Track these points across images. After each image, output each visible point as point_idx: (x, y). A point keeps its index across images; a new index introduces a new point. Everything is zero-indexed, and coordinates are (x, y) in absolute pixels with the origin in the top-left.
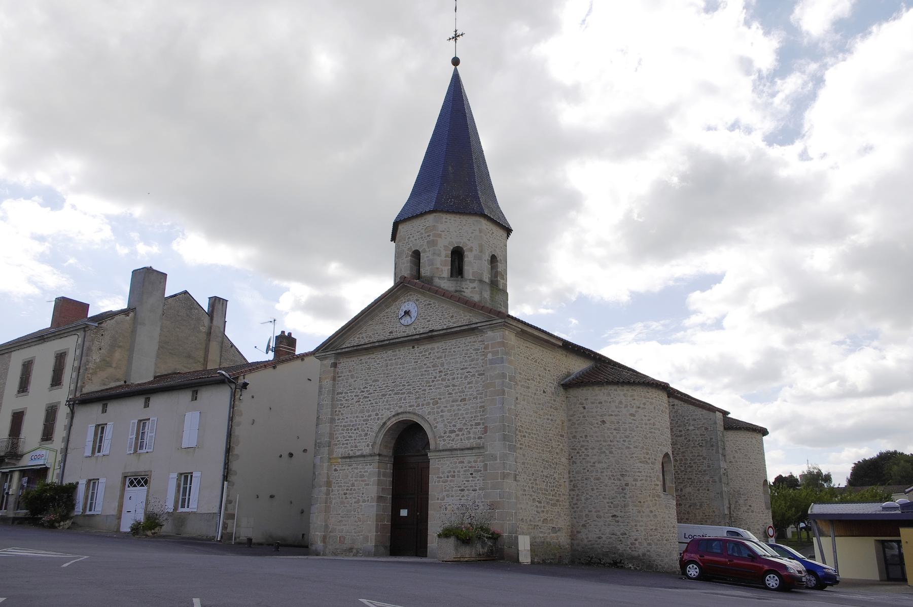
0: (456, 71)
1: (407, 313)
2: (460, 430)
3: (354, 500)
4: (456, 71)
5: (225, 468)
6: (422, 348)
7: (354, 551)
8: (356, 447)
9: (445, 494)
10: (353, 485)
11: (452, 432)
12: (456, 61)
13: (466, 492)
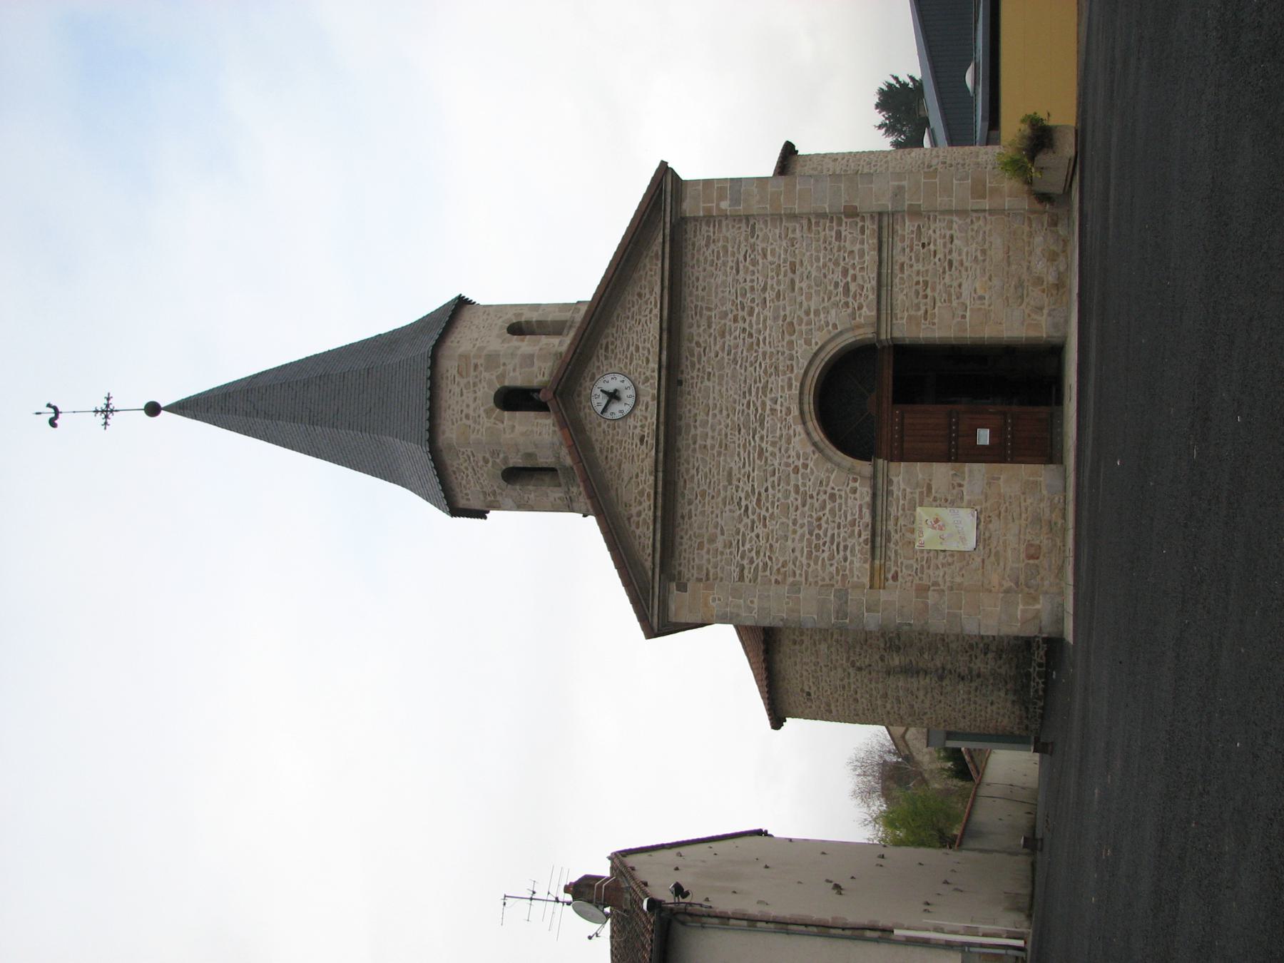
1: (614, 396)
8: (853, 523)
12: (153, 409)
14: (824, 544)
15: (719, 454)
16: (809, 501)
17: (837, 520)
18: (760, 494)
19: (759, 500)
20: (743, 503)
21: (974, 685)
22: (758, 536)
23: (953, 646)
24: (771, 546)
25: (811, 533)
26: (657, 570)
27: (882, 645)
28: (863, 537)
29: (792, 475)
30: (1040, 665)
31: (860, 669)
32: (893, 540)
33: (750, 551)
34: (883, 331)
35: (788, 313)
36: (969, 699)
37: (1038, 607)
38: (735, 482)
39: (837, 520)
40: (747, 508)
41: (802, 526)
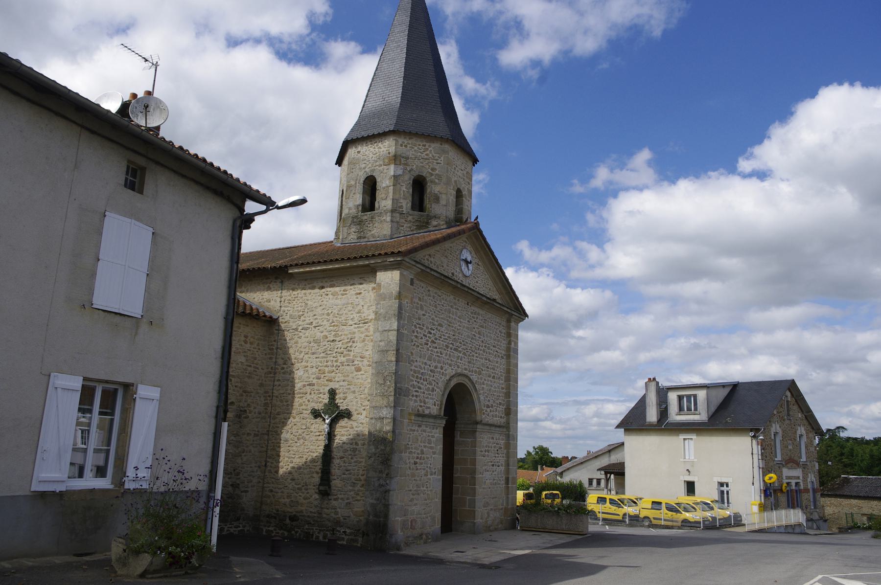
7: (424, 536)
27: (241, 404)
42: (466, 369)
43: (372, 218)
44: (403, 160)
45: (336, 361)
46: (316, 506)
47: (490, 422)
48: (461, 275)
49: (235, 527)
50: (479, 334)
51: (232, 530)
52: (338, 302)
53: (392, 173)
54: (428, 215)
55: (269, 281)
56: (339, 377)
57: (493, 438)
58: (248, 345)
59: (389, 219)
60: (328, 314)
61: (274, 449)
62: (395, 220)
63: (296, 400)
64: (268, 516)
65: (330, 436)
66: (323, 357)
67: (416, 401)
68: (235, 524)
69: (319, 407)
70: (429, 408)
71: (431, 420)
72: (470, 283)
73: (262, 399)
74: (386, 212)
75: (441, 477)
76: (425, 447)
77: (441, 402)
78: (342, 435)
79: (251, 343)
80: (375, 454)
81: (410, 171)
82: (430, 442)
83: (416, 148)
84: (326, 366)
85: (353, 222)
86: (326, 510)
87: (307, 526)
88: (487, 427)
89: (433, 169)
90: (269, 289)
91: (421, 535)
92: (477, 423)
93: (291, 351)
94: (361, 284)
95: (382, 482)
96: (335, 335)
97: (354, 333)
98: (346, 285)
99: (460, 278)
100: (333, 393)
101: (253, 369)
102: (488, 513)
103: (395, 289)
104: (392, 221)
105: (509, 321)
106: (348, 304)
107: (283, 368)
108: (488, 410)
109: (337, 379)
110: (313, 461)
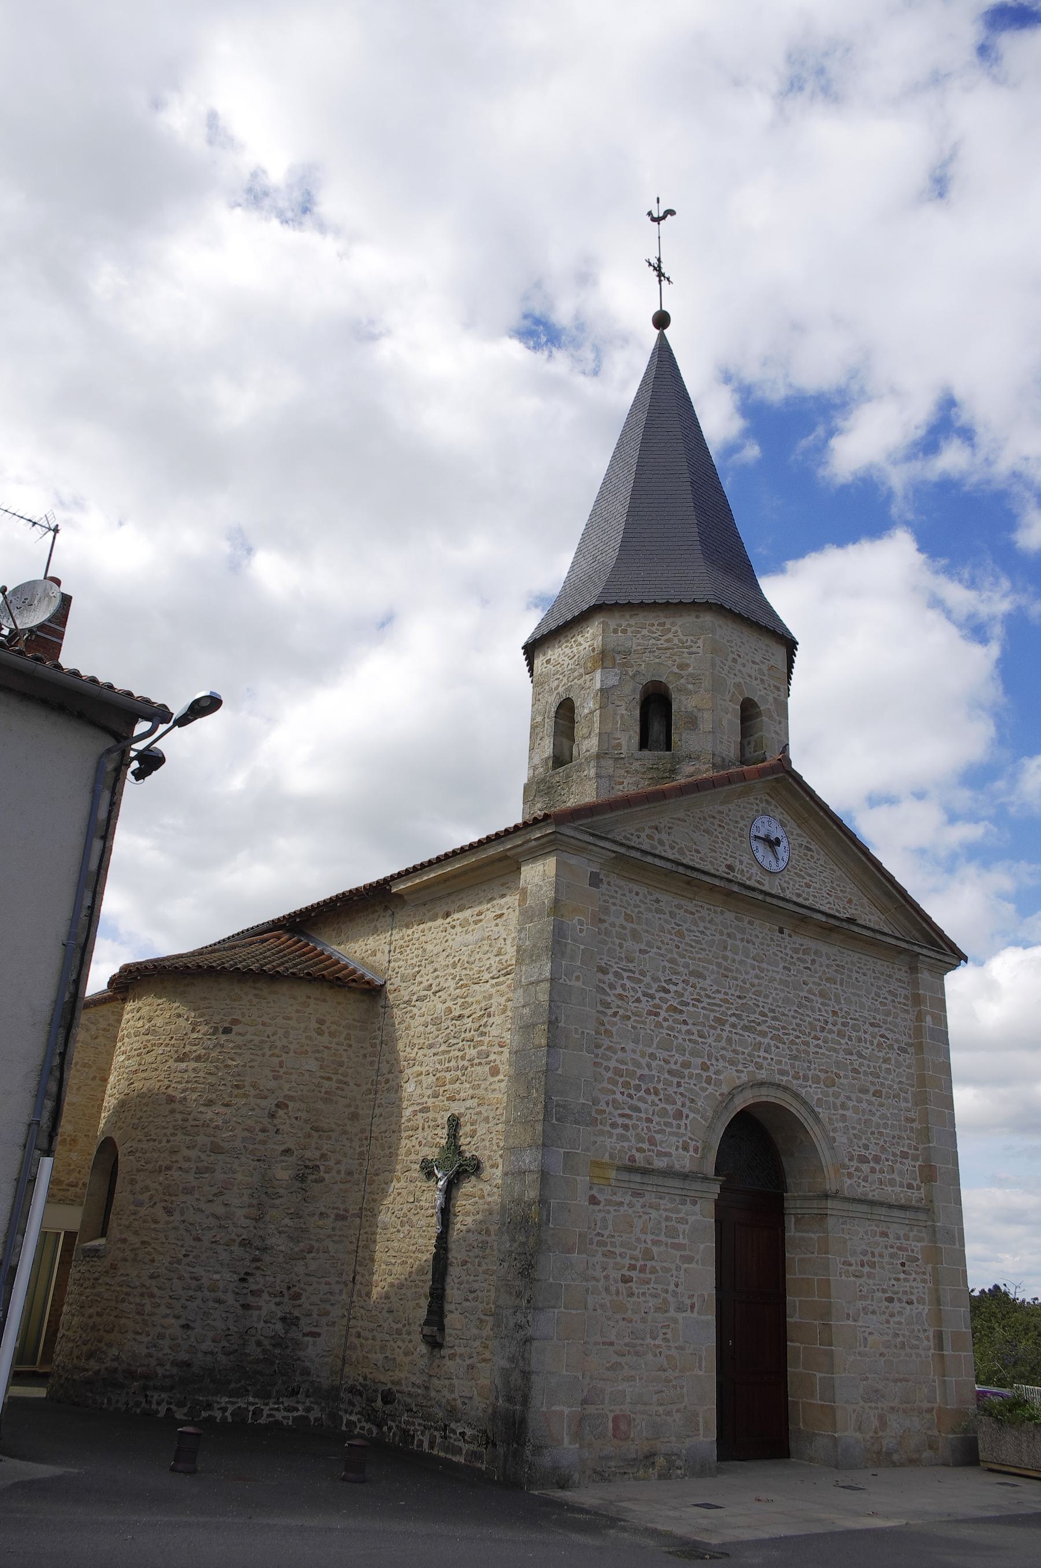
0: (662, 338)
1: (772, 844)
2: (877, 1159)
3: (652, 1303)
4: (662, 338)
5: (41, 1093)
6: (798, 940)
7: (660, 1461)
8: (652, 1142)
9: (860, 1304)
10: (648, 1255)
11: (863, 1159)
12: (662, 320)
13: (896, 1305)
14: (630, 1096)
15: (719, 965)
16: (675, 1080)
17: (656, 1119)
18: (681, 1012)
19: (675, 1010)
20: (672, 988)
21: (230, 1298)
22: (638, 1000)
23: (300, 1268)
24: (629, 1018)
25: (642, 1078)
26: (622, 850)
27: (308, 1154)
28: (638, 1155)
29: (699, 1061)
30: (258, 1413)
31: (272, 1116)
32: (634, 1200)
33: (623, 986)
34: (798, 1204)
35: (842, 1081)
36: (199, 1288)
37: (566, 1440)
38: (692, 980)
39: (656, 1119)
40: (667, 991)
41: (649, 1066)
42: (782, 1072)
43: (568, 776)
44: (618, 657)
45: (463, 1058)
46: (422, 1372)
47: (874, 1195)
48: (755, 870)
49: (287, 1409)
50: (822, 994)
51: (279, 1416)
52: (470, 938)
53: (598, 686)
54: (673, 757)
55: (376, 916)
56: (466, 1089)
57: (884, 1234)
58: (325, 1039)
59: (592, 772)
60: (454, 965)
61: (366, 1247)
62: (604, 772)
63: (404, 1142)
64: (352, 1390)
65: (446, 1213)
66: (444, 1052)
67: (622, 1138)
68: (287, 1402)
69: (432, 1153)
70: (668, 1154)
71: (677, 1183)
72: (791, 888)
73: (356, 1144)
74: (588, 760)
75: (711, 1318)
76: (655, 1243)
77: (706, 1147)
78: (467, 1214)
79: (332, 1035)
80: (511, 1252)
81: (634, 677)
82: (672, 1233)
83: (645, 632)
84: (448, 1070)
85: (538, 791)
86: (435, 1381)
87: (405, 1418)
88: (864, 1208)
89: (682, 666)
90: (375, 931)
91: (650, 1457)
92: (826, 1196)
93: (400, 1045)
94: (503, 896)
95: (520, 1318)
96: (463, 1006)
97: (491, 996)
98: (481, 903)
99: (753, 877)
100: (454, 1123)
101: (334, 1085)
102: (882, 1418)
103: (548, 894)
104: (598, 776)
105: (913, 969)
106: (483, 939)
107: (387, 1081)
108: (865, 1167)
109: (463, 1095)
110: (421, 1271)
